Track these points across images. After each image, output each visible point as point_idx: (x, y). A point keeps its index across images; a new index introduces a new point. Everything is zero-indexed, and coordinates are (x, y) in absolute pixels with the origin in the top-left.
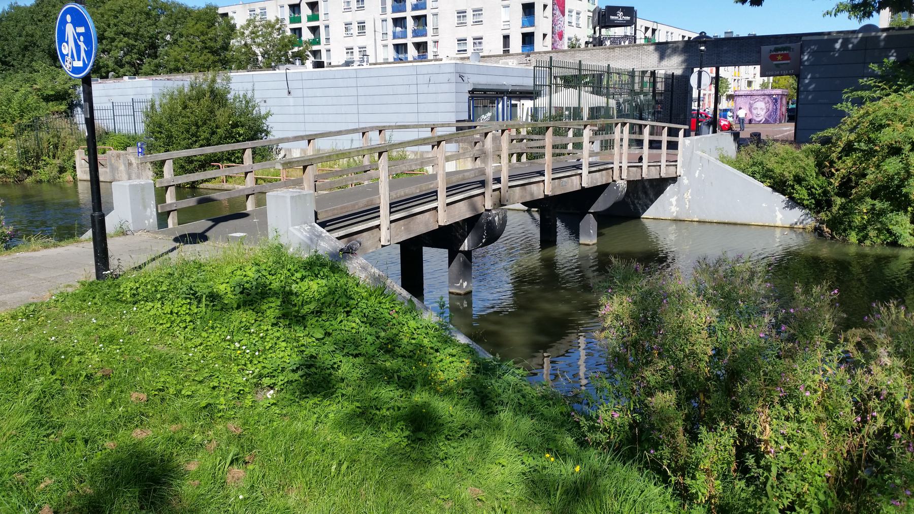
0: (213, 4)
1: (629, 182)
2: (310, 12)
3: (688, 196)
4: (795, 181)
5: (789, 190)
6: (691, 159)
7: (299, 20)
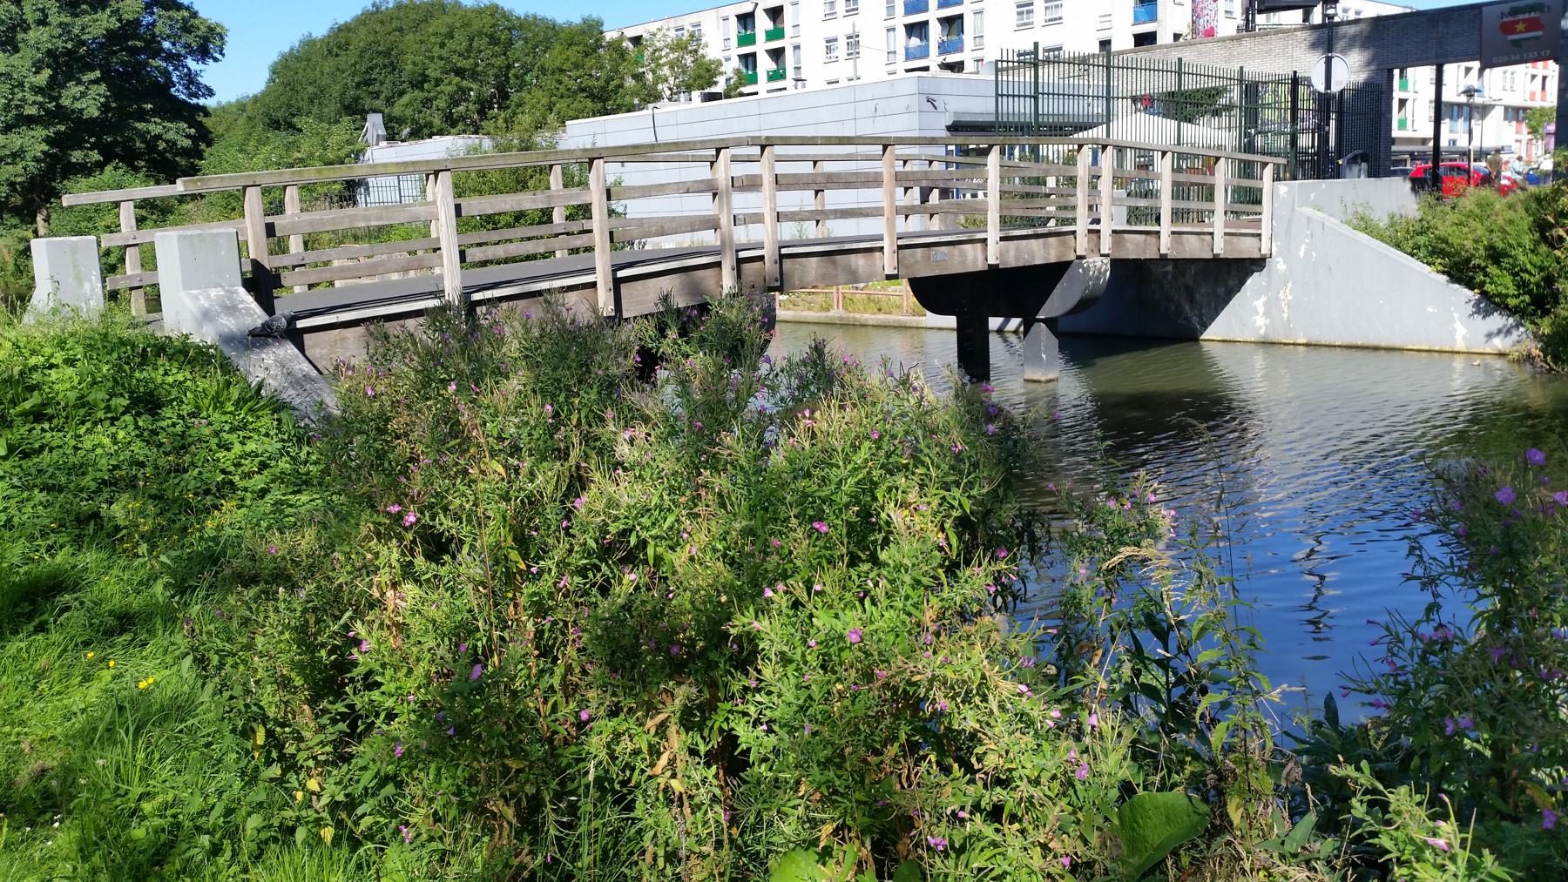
0: (595, 16)
1: (1116, 264)
2: (769, 25)
3: (1285, 295)
4: (1488, 257)
5: (1480, 278)
6: (1290, 221)
7: (751, 40)
